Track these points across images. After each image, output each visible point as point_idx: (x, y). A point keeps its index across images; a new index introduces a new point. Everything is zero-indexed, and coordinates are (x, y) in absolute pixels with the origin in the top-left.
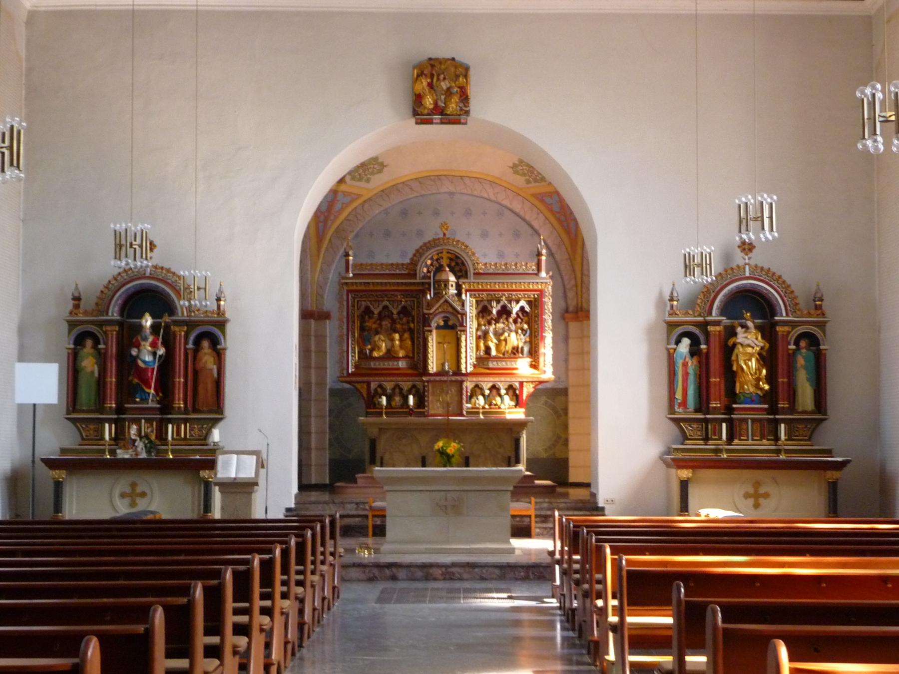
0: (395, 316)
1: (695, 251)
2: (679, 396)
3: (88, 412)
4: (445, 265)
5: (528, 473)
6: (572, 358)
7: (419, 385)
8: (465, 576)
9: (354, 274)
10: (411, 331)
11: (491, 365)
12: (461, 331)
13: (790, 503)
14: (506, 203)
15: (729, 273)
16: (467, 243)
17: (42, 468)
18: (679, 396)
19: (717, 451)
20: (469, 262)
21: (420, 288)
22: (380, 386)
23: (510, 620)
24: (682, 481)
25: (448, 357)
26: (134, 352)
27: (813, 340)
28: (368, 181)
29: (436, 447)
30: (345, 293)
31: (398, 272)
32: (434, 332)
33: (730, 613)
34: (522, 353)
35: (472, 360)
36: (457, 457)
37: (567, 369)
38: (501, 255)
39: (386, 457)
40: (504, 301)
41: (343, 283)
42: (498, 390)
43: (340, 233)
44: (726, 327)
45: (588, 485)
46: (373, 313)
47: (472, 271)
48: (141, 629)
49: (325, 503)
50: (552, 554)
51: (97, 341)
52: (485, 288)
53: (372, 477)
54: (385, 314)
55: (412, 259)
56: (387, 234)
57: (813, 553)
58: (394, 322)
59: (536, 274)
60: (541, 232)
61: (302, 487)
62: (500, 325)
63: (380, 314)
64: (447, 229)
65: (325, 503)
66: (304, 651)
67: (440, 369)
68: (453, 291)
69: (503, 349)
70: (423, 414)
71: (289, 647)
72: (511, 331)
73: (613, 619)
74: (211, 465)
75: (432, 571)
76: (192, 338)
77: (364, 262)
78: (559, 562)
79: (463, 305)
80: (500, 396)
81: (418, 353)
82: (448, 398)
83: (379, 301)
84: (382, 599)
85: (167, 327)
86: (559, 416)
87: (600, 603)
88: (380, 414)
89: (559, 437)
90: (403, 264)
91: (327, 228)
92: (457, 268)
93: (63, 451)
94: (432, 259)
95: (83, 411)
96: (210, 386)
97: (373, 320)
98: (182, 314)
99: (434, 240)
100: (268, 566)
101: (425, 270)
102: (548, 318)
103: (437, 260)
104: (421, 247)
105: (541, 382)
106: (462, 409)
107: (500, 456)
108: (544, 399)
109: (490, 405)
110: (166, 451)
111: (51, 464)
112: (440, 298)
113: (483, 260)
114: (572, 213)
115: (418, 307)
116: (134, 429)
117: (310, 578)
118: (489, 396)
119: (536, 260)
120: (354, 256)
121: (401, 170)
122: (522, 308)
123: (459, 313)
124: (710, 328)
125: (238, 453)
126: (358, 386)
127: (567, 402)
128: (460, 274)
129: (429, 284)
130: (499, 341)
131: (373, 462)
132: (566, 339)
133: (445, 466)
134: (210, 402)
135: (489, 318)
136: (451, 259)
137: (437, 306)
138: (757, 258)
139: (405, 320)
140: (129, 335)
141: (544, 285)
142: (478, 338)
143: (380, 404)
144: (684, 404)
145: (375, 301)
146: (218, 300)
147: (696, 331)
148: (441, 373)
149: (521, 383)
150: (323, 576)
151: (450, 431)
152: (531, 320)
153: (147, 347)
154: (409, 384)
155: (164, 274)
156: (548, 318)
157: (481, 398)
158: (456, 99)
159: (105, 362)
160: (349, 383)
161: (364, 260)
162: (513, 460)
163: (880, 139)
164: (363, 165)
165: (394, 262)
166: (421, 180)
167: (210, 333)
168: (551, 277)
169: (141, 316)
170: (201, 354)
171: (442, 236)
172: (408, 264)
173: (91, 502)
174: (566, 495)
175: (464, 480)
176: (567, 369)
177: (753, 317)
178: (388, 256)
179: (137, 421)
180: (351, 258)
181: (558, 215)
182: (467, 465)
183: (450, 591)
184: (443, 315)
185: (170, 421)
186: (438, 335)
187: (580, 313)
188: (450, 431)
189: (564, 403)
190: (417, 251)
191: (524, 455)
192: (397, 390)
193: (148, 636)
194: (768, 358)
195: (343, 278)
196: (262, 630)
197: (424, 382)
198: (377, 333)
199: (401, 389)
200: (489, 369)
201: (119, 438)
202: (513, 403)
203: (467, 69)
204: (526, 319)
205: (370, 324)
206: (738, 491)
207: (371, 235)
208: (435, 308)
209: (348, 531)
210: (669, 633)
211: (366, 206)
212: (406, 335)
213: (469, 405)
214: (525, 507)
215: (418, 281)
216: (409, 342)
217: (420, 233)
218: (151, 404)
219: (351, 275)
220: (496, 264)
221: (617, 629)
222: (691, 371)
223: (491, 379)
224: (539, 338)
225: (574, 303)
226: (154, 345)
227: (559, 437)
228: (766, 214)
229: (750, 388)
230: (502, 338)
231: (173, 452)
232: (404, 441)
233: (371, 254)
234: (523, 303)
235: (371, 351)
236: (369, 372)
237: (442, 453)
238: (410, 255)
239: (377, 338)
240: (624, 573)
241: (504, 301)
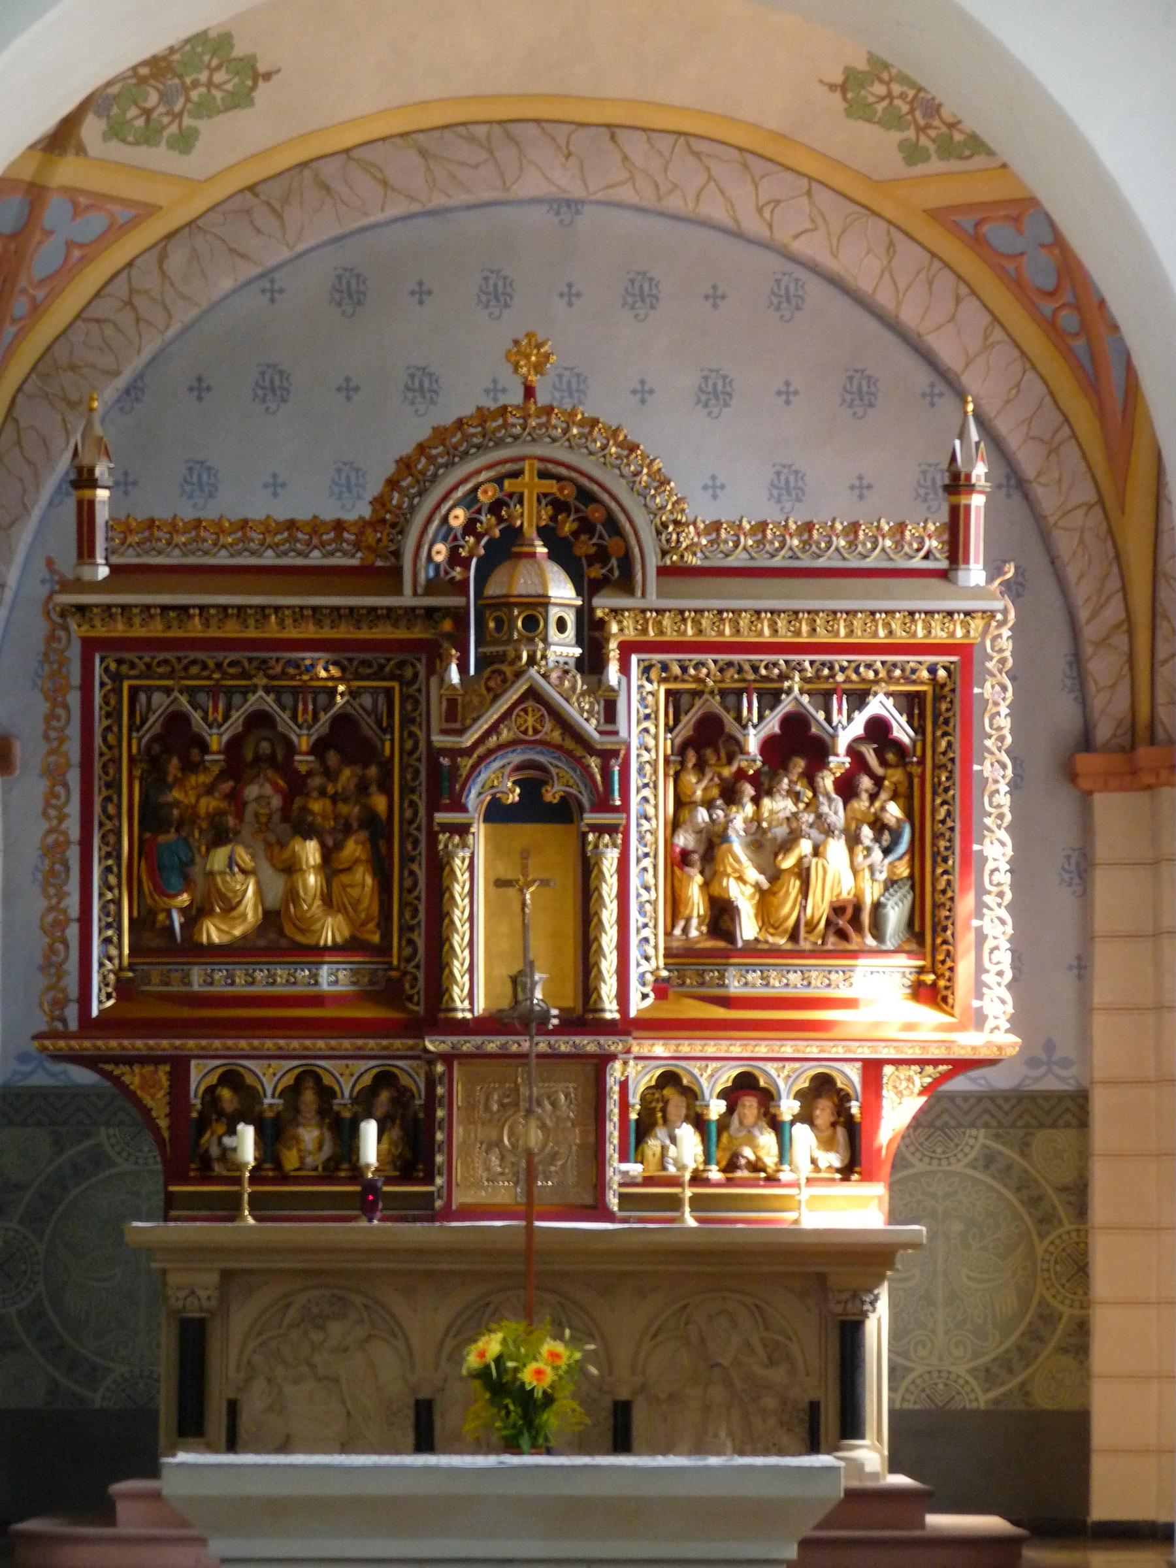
0: (304, 762)
4: (530, 532)
5: (900, 1480)
6: (1104, 956)
7: (411, 1075)
9: (114, 569)
10: (376, 829)
11: (735, 986)
12: (600, 829)
14: (811, 247)
16: (628, 432)
20: (641, 519)
21: (418, 633)
22: (231, 1079)
25: (539, 947)
28: (185, 142)
29: (472, 1361)
30: (74, 653)
31: (315, 558)
32: (480, 830)
34: (877, 929)
35: (647, 963)
36: (566, 1403)
37: (1085, 1009)
38: (787, 485)
39: (254, 1405)
40: (797, 696)
42: (768, 1098)
46: (205, 748)
47: (653, 561)
52: (711, 636)
53: (156, 1496)
55: (380, 502)
56: (273, 386)
58: (296, 786)
59: (943, 574)
60: (968, 380)
62: (779, 806)
63: (233, 747)
64: (538, 368)
67: (505, 1003)
68: (563, 648)
69: (788, 910)
70: (423, 1209)
72: (829, 832)
77: (162, 513)
79: (610, 713)
80: (776, 1125)
81: (406, 929)
82: (534, 1137)
83: (230, 692)
86: (1046, 1221)
88: (228, 1207)
89: (1047, 1317)
90: (339, 526)
92: (585, 547)
94: (470, 501)
97: (204, 778)
99: (483, 416)
101: (441, 552)
103: (495, 507)
104: (421, 448)
105: (961, 1066)
106: (600, 1185)
107: (770, 1402)
108: (978, 1140)
109: (731, 1166)
112: (505, 684)
113: (701, 510)
114: (1102, 303)
115: (407, 720)
118: (723, 1124)
119: (944, 516)
120: (122, 485)
122: (878, 729)
123: (591, 750)
126: (132, 1078)
127: (1084, 1154)
128: (596, 572)
129: (460, 616)
130: (775, 876)
131: (190, 1428)
132: (1083, 867)
133: (512, 1447)
135: (727, 772)
136: (559, 506)
137: (493, 715)
139: (347, 776)
141: (977, 625)
142: (680, 860)
143: (228, 1155)
145: (213, 692)
149: (872, 1069)
151: (531, 1281)
152: (917, 776)
154: (363, 1071)
156: (994, 771)
157: (687, 1134)
161: (164, 502)
162: (830, 1418)
164: (158, 68)
165: (303, 515)
168: (1014, 589)
171: (515, 397)
172: (364, 525)
176: (1085, 1009)
178: (275, 486)
180: (102, 494)
181: (1048, 307)
182: (622, 1443)
184: (516, 758)
186: (496, 850)
187: (1144, 753)
188: (531, 1281)
190: (406, 465)
192: (309, 1097)
195: (67, 586)
197: (431, 1059)
198: (220, 836)
199: (326, 1094)
200: (727, 1002)
202: (832, 1159)
204: (895, 776)
205: (188, 794)
207: (200, 388)
208: (484, 725)
211: (177, 259)
212: (353, 848)
213: (635, 1169)
215: (407, 599)
216: (364, 880)
217: (422, 385)
219: (103, 572)
220: (762, 526)
223: (736, 1050)
224: (955, 861)
225: (1121, 705)
227: (1047, 1317)
230: (788, 862)
232: (336, 1328)
233: (200, 477)
235: (195, 916)
236: (186, 1013)
237: (499, 1384)
238: (374, 486)
239: (219, 857)
241: (797, 696)
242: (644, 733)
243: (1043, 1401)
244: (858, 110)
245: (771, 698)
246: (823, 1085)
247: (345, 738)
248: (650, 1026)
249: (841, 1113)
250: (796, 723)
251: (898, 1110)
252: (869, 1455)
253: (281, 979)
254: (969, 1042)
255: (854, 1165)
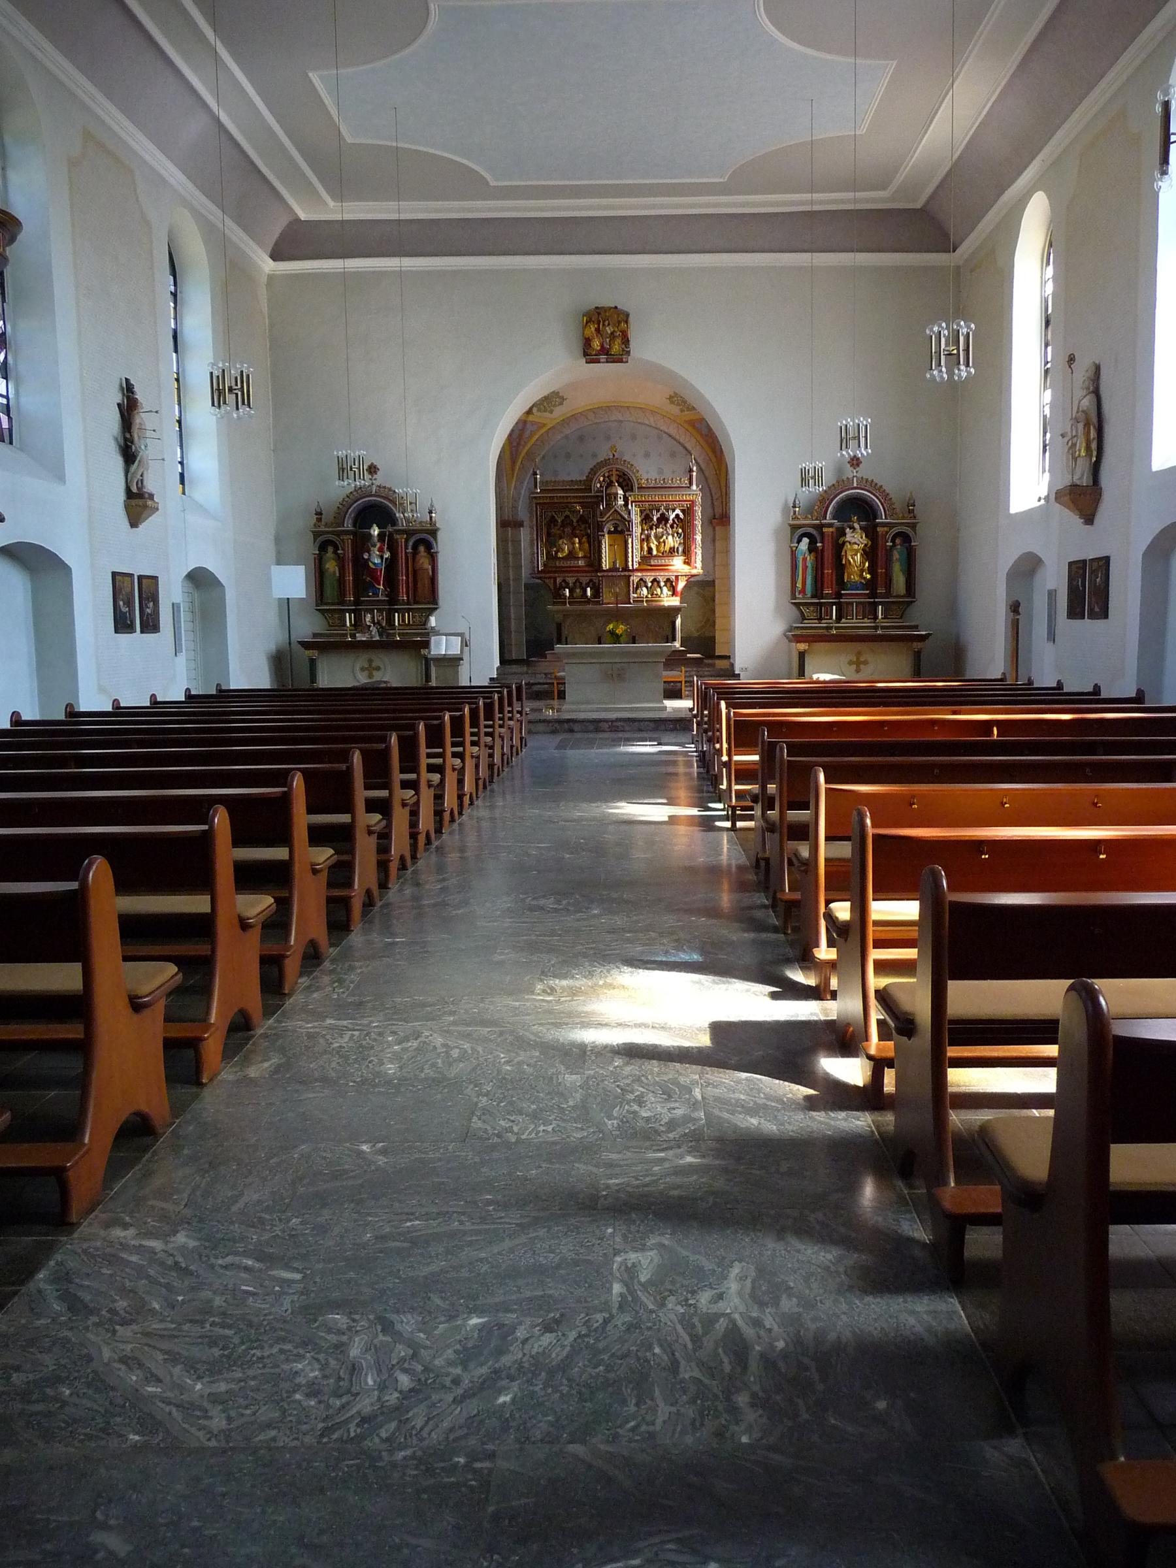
1: (809, 466)
2: (799, 585)
3: (333, 604)
8: (627, 728)
10: (589, 536)
13: (886, 671)
14: (664, 428)
15: (841, 484)
17: (297, 648)
18: (799, 585)
19: (828, 628)
22: (564, 581)
23: (665, 760)
24: (800, 653)
26: (366, 556)
27: (906, 538)
28: (551, 412)
33: (793, 749)
38: (661, 471)
40: (663, 510)
41: (533, 498)
42: (658, 582)
43: (530, 456)
44: (837, 529)
45: (728, 657)
48: (344, 767)
49: (522, 674)
50: (691, 710)
51: (336, 548)
54: (567, 522)
57: (886, 705)
58: (574, 529)
61: (503, 661)
65: (522, 674)
66: (495, 786)
68: (621, 502)
69: (662, 549)
70: (598, 603)
71: (481, 782)
73: (725, 758)
74: (426, 645)
75: (601, 724)
76: (411, 544)
78: (695, 716)
84: (561, 746)
85: (391, 535)
87: (718, 746)
91: (518, 451)
93: (315, 635)
95: (326, 604)
96: (427, 582)
98: (402, 525)
100: (457, 724)
102: (698, 523)
110: (394, 635)
111: (306, 645)
113: (645, 476)
116: (368, 617)
117: (498, 730)
121: (578, 402)
122: (677, 515)
124: (825, 530)
125: (446, 635)
131: (559, 642)
134: (427, 595)
138: (863, 471)
140: (362, 542)
143: (564, 595)
144: (803, 591)
146: (431, 512)
147: (814, 532)
148: (613, 569)
149: (677, 577)
150: (511, 729)
151: (618, 615)
152: (685, 525)
153: (375, 551)
154: (588, 579)
155: (387, 493)
156: (698, 523)
157: (644, 589)
158: (618, 341)
159: (343, 566)
160: (540, 578)
161: (549, 478)
163: (944, 369)
164: (546, 398)
166: (594, 411)
167: (424, 539)
169: (370, 527)
170: (418, 557)
173: (338, 674)
174: (713, 665)
175: (629, 654)
177: (859, 520)
179: (371, 611)
183: (613, 740)
185: (397, 610)
189: (709, 593)
191: (679, 635)
193: (349, 772)
194: (870, 553)
196: (454, 770)
201: (358, 625)
203: (628, 315)
205: (554, 530)
206: (844, 659)
209: (538, 696)
210: (756, 767)
212: (584, 539)
214: (677, 675)
217: (594, 456)
218: (381, 598)
221: (727, 765)
222: (809, 565)
226: (381, 550)
228: (862, 434)
229: (855, 578)
231: (399, 635)
234: (678, 511)
235: (556, 553)
240: (732, 723)
242: (636, 518)
243: (707, 634)
244: (672, 403)
245: (658, 511)
246: (668, 580)
247: (582, 520)
248: (637, 570)
249: (671, 584)
250: (663, 515)
251: (681, 585)
252: (677, 644)
253: (572, 563)
254: (694, 572)
255: (674, 593)
